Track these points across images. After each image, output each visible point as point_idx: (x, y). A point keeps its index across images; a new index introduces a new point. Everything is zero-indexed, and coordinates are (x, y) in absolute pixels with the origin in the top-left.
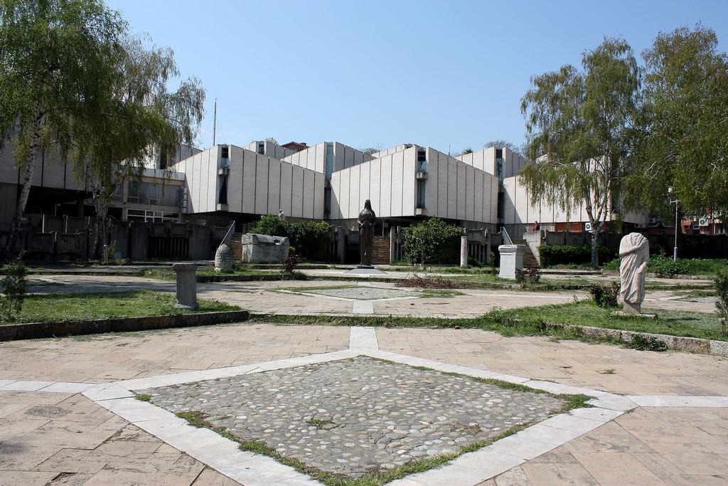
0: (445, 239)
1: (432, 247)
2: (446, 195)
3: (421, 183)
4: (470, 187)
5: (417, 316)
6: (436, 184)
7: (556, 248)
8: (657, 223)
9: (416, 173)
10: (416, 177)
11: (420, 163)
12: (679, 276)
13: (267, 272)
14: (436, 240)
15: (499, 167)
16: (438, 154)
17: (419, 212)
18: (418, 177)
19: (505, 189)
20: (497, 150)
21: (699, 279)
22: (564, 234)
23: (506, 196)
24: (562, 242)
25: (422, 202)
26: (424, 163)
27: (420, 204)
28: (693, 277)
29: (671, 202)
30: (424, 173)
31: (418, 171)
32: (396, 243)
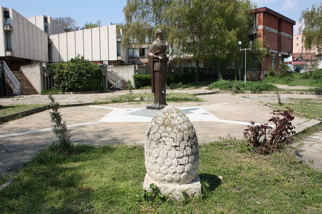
0: (95, 72)
1: (85, 78)
2: (23, 43)
3: (8, 34)
4: (35, 39)
5: (132, 144)
6: (18, 35)
7: (144, 76)
8: (132, 61)
9: (4, 26)
10: (4, 30)
11: (5, 19)
12: (264, 92)
13: (21, 138)
14: (88, 72)
15: (46, 28)
16: (18, 14)
17: (9, 54)
18: (5, 29)
19: (52, 41)
20: (44, 18)
21: (157, 86)
22: (146, 67)
23: (52, 45)
24: (145, 72)
25: (9, 47)
26: (8, 19)
27: (8, 49)
28: (271, 92)
29: (241, 50)
30: (10, 25)
31: (5, 25)
32: (44, 76)
